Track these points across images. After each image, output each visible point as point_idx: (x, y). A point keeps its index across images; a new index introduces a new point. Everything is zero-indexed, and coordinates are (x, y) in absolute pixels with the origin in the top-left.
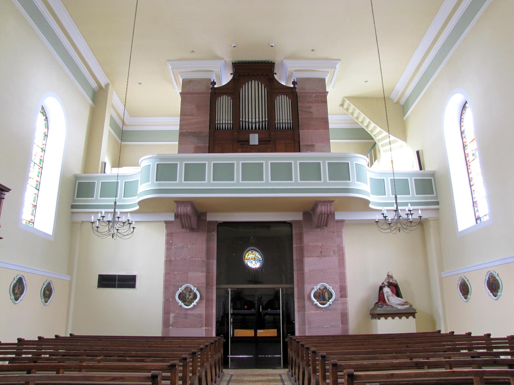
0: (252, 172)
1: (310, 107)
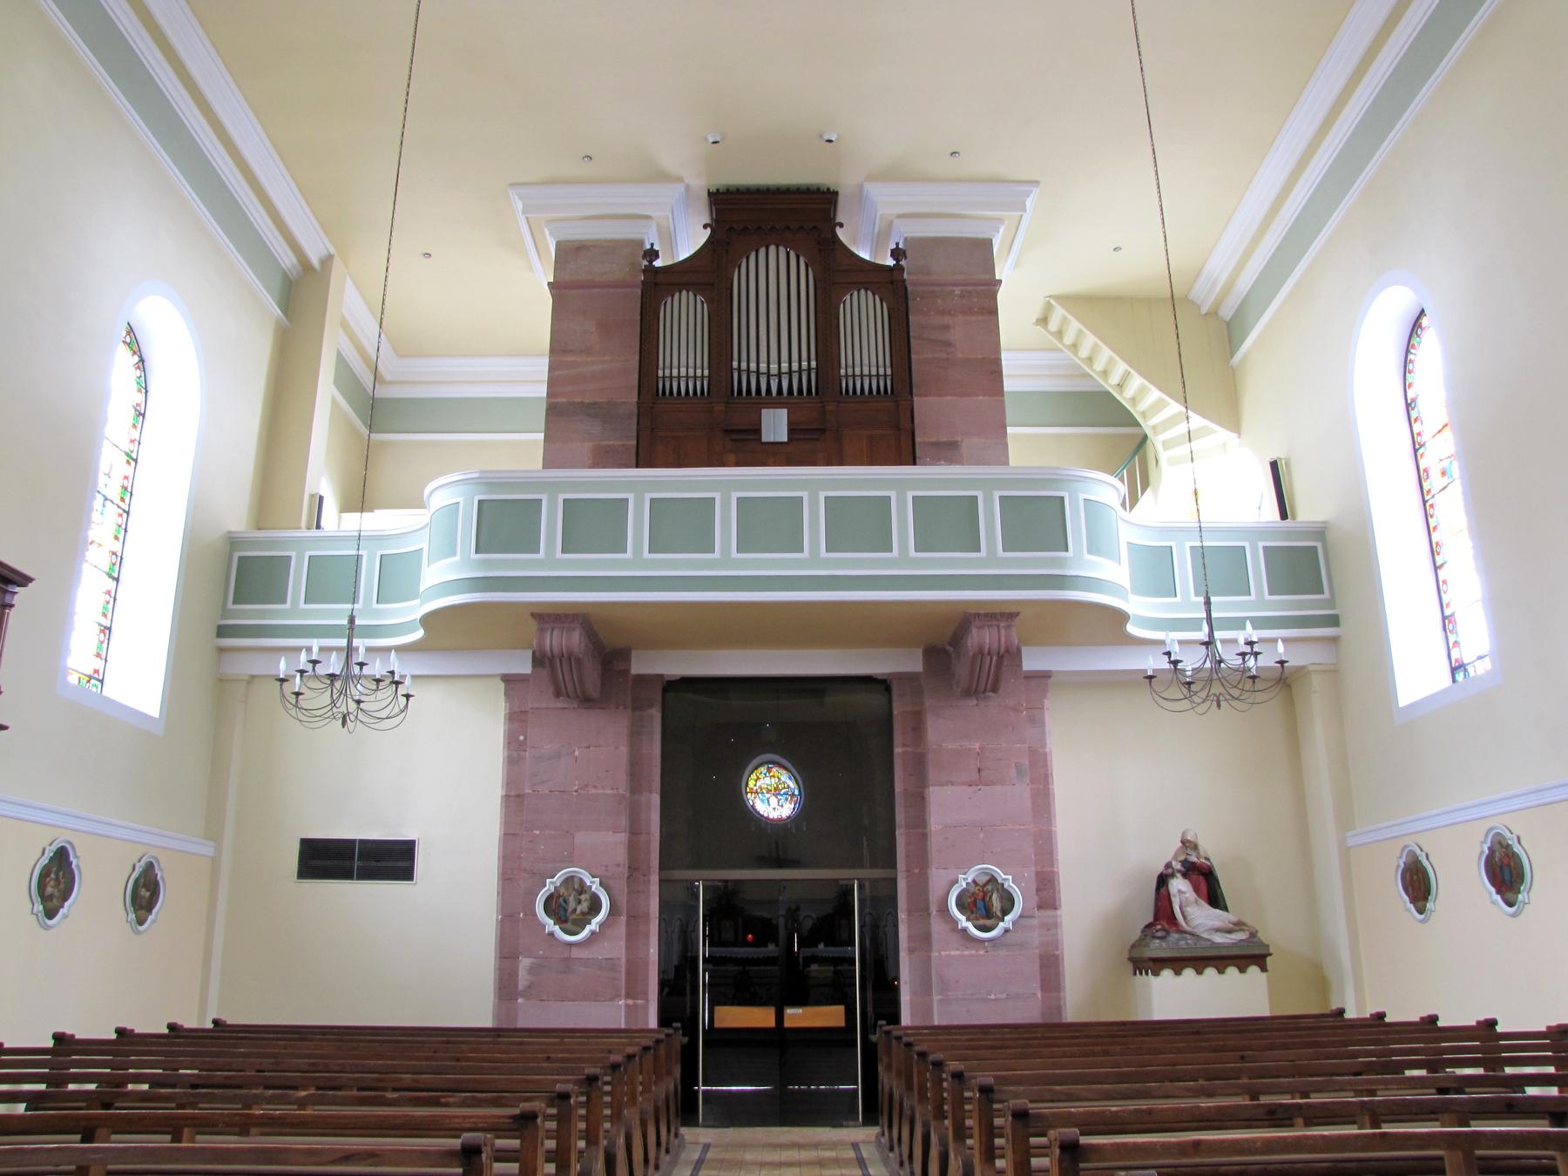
0: (770, 525)
1: (946, 327)
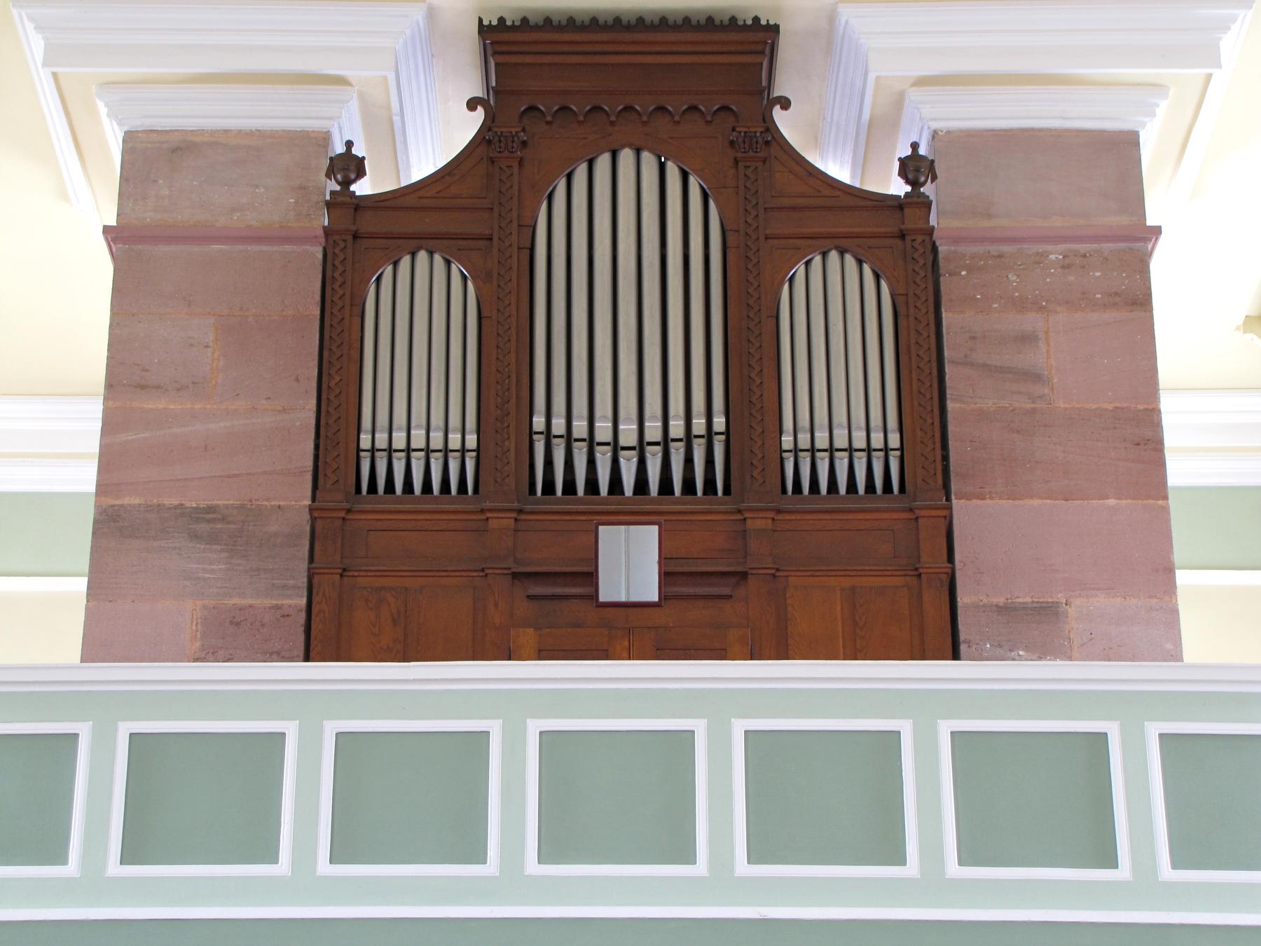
1: (1026, 339)
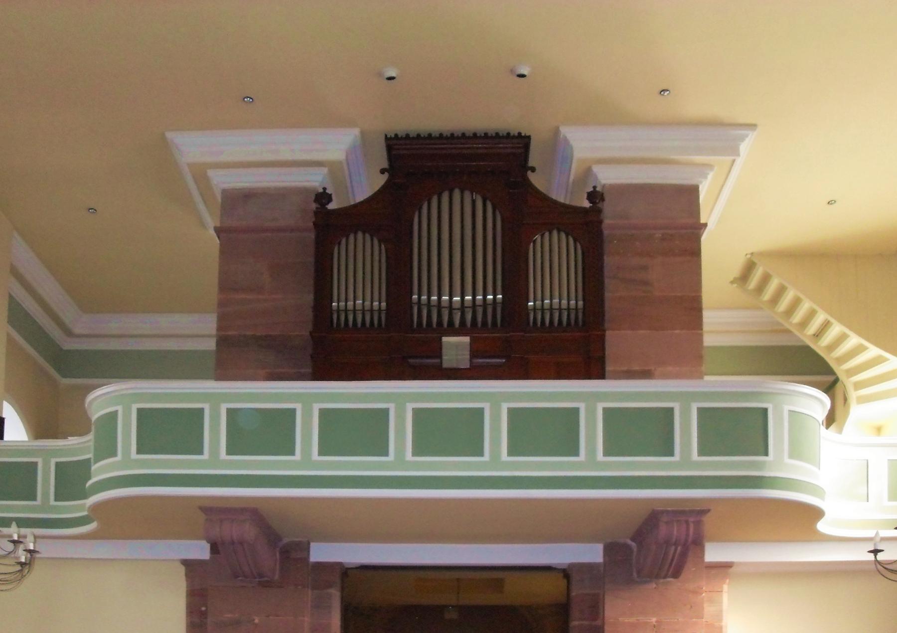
0: (451, 433)
1: (645, 268)
